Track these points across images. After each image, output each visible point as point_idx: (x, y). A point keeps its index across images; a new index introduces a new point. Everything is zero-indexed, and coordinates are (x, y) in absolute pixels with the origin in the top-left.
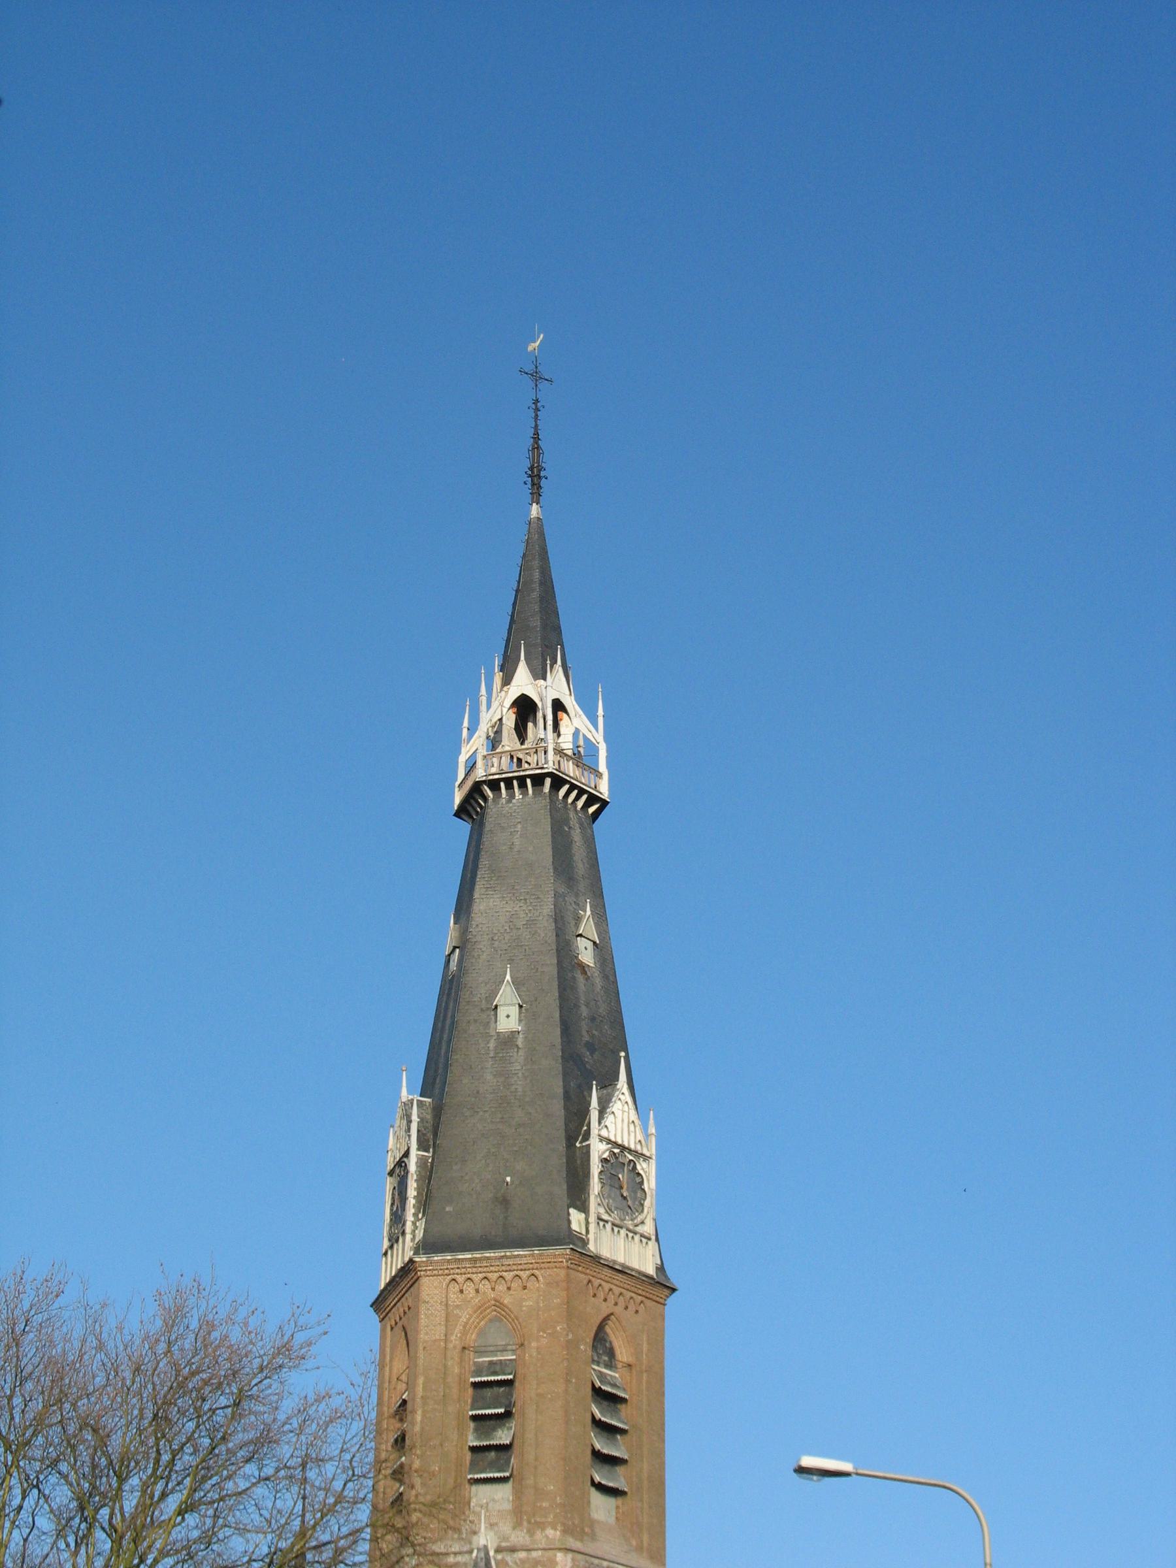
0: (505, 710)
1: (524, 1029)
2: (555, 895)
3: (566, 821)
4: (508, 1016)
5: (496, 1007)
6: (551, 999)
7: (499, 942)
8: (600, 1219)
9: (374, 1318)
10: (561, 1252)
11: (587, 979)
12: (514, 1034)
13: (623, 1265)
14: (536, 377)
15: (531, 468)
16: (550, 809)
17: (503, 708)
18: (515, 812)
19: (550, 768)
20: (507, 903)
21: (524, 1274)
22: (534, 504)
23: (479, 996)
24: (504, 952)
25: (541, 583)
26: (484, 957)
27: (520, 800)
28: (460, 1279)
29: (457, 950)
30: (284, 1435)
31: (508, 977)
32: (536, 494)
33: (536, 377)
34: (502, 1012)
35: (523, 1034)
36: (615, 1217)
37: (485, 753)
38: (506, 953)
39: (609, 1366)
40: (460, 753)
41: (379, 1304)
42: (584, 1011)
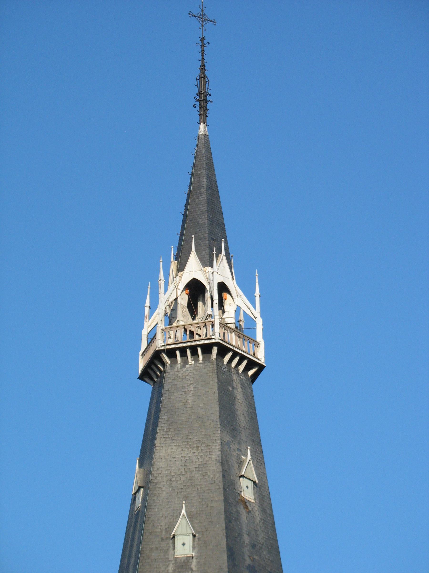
0: (179, 292)
1: (197, 555)
2: (221, 443)
4: (184, 544)
5: (174, 537)
7: (176, 482)
11: (249, 512)
12: (188, 559)
16: (217, 372)
17: (178, 290)
18: (188, 375)
20: (182, 450)
22: (202, 124)
23: (160, 527)
24: (180, 490)
26: (164, 494)
27: (192, 366)
29: (142, 490)
30: (253, 454)
31: (184, 512)
34: (179, 541)
35: (196, 559)
37: (164, 327)
38: (181, 492)
40: (143, 327)
42: (246, 539)
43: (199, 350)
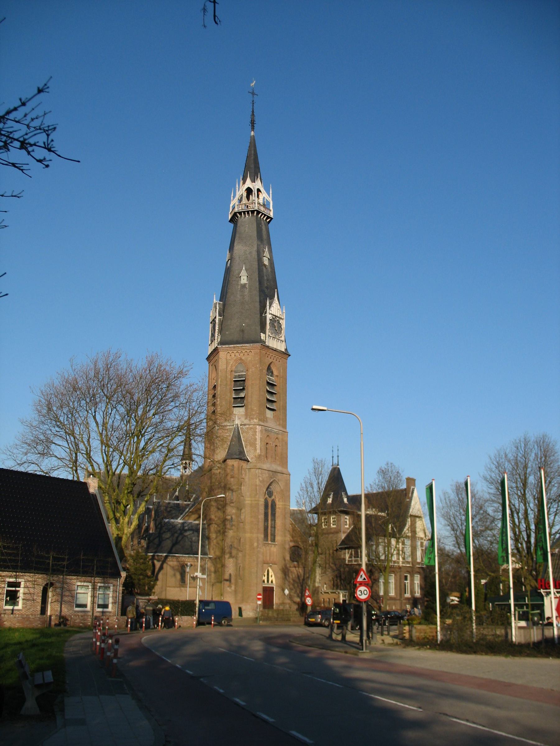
3: (261, 224)
6: (256, 275)
8: (269, 336)
9: (207, 362)
10: (259, 345)
11: (266, 269)
13: (276, 349)
14: (253, 94)
15: (252, 121)
19: (256, 208)
21: (248, 351)
25: (254, 155)
28: (230, 352)
31: (244, 268)
32: (253, 128)
33: (253, 94)
34: (242, 278)
36: (273, 335)
39: (272, 376)
41: (208, 359)
42: (265, 278)
43: (250, 212)
